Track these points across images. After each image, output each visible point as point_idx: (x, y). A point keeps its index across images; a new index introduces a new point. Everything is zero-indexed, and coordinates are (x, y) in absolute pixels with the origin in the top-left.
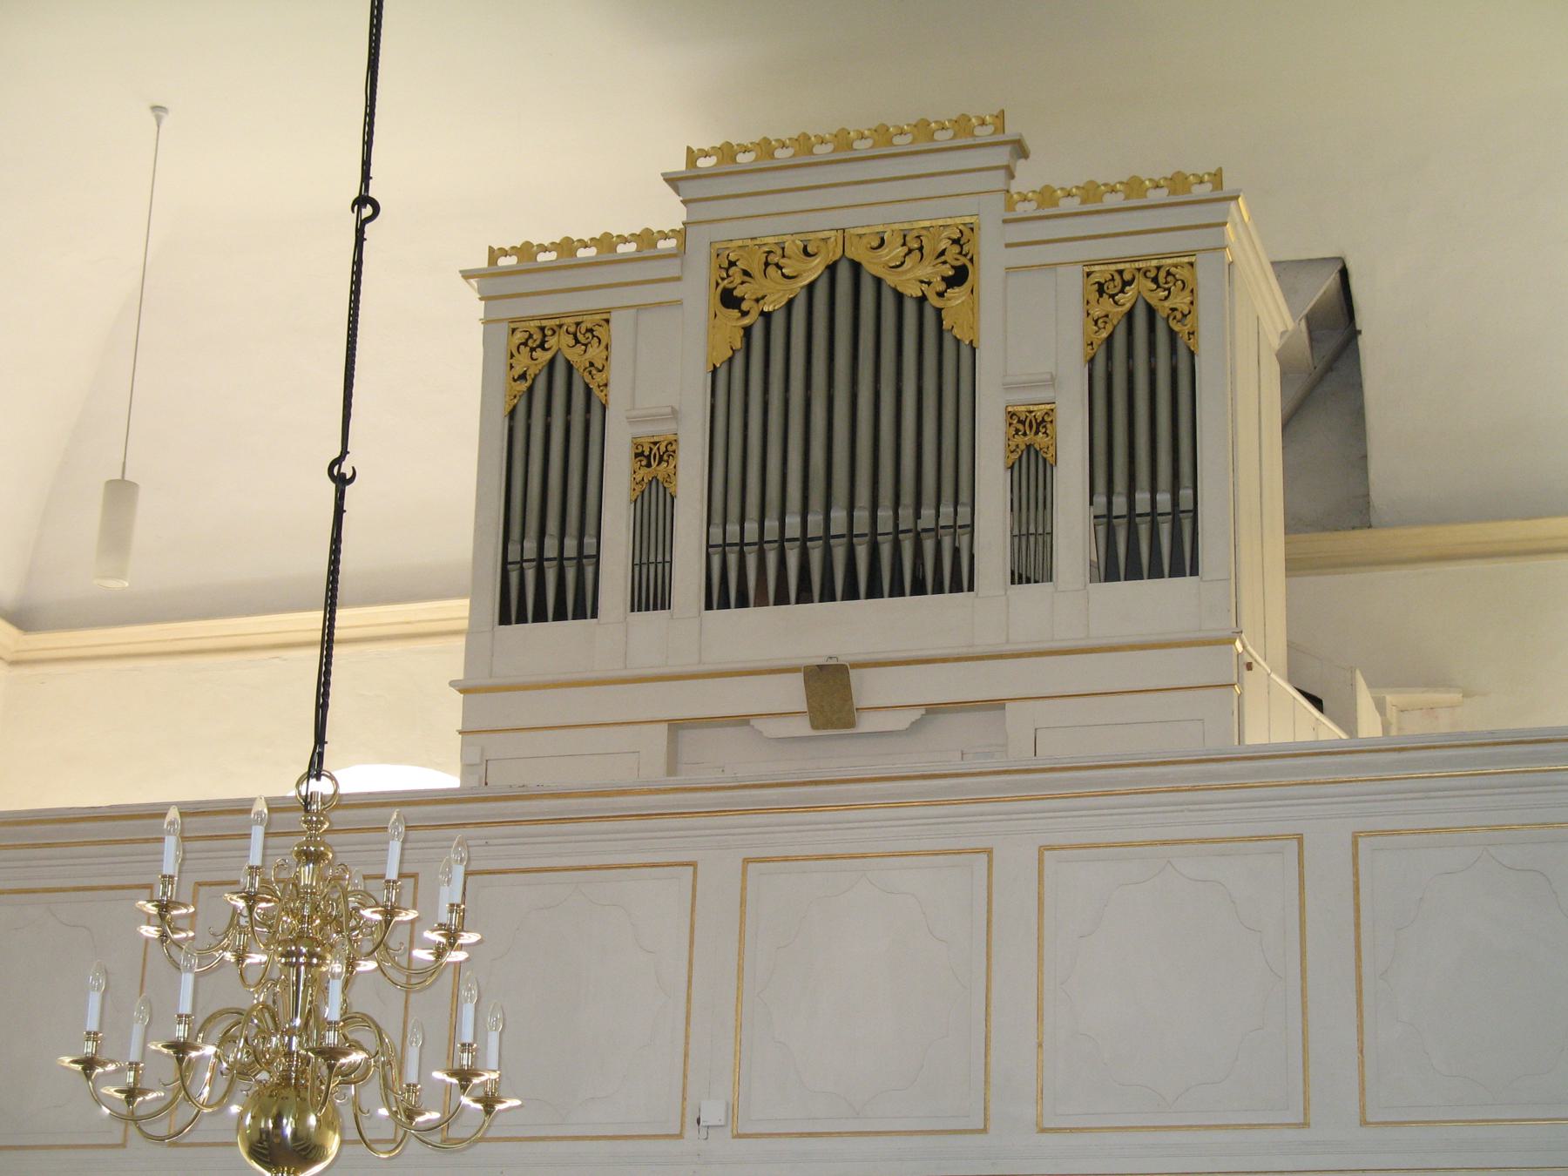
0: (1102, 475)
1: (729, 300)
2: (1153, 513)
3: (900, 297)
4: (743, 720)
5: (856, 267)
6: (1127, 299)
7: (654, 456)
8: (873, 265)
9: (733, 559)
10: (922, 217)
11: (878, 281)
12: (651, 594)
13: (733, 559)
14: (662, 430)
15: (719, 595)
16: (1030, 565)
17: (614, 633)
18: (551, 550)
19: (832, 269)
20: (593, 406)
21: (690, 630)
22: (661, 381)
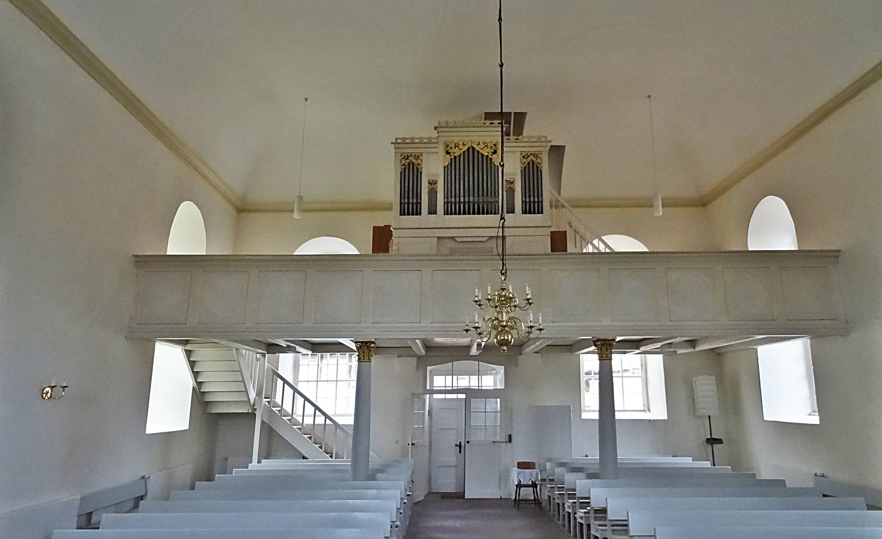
0: (524, 195)
1: (448, 153)
2: (534, 202)
3: (482, 155)
4: (453, 238)
5: (474, 148)
6: (529, 159)
7: (432, 183)
8: (477, 148)
9: (467, 206)
10: (467, 139)
11: (478, 152)
12: (433, 211)
13: (467, 206)
14: (434, 178)
15: (446, 213)
16: (433, 211)
17: (425, 218)
18: (411, 201)
19: (468, 148)
20: (419, 173)
21: (440, 219)
22: (434, 167)
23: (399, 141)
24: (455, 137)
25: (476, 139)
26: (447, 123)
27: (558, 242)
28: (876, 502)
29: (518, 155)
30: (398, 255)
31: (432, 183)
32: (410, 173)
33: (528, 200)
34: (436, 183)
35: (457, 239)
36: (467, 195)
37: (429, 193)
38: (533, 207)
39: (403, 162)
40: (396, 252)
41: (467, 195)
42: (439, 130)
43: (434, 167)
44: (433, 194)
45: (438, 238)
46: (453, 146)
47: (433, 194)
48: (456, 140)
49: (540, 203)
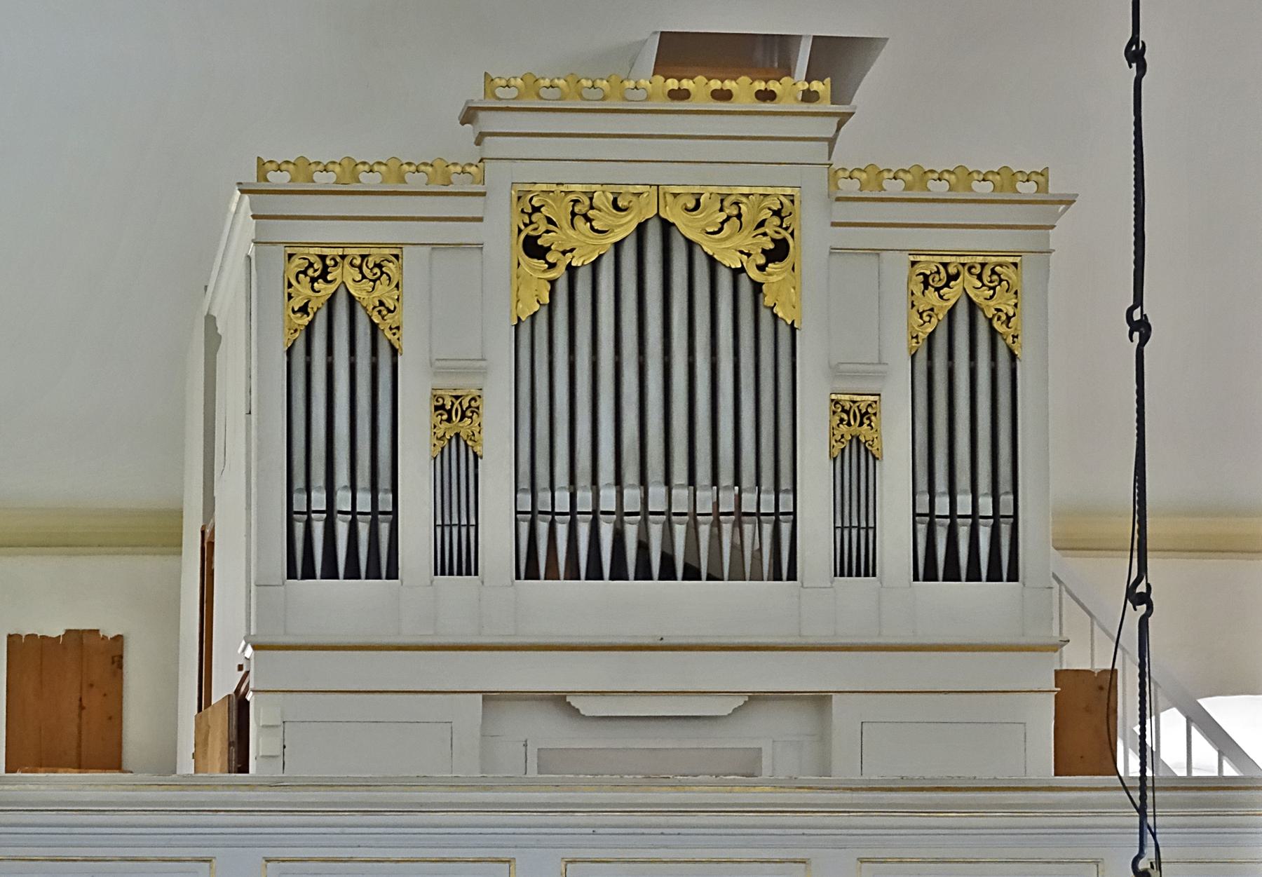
1: (534, 249)
3: (713, 263)
4: (560, 700)
6: (953, 293)
7: (854, 415)
11: (690, 244)
14: (466, 386)
18: (343, 501)
19: (641, 229)
20: (383, 352)
22: (460, 326)
23: (279, 179)
24: (559, 165)
25: (685, 181)
26: (532, 82)
27: (1087, 720)
28: (1258, 788)
29: (898, 274)
30: (276, 785)
31: (854, 415)
32: (338, 343)
33: (942, 506)
34: (470, 410)
35: (587, 707)
36: (631, 475)
37: (440, 459)
38: (973, 548)
39: (303, 290)
40: (275, 771)
41: (631, 475)
42: (489, 122)
43: (460, 326)
44: (458, 467)
45: (489, 697)
46: (561, 213)
47: (458, 467)
48: (577, 180)
49: (1007, 523)
